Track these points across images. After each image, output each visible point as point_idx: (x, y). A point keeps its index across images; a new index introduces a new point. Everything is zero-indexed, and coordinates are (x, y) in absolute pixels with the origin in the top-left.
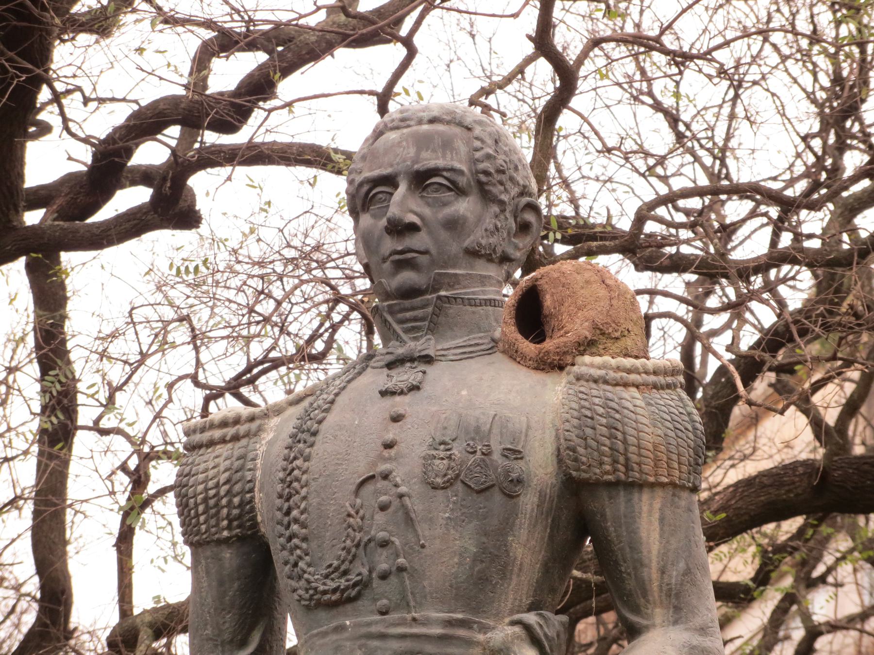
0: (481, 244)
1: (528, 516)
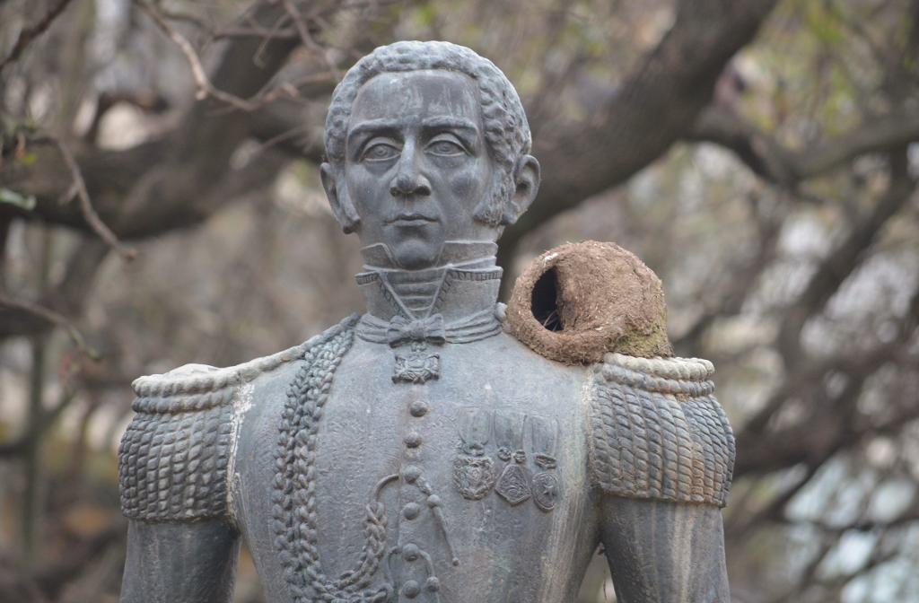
0: (489, 212)
1: (559, 532)
